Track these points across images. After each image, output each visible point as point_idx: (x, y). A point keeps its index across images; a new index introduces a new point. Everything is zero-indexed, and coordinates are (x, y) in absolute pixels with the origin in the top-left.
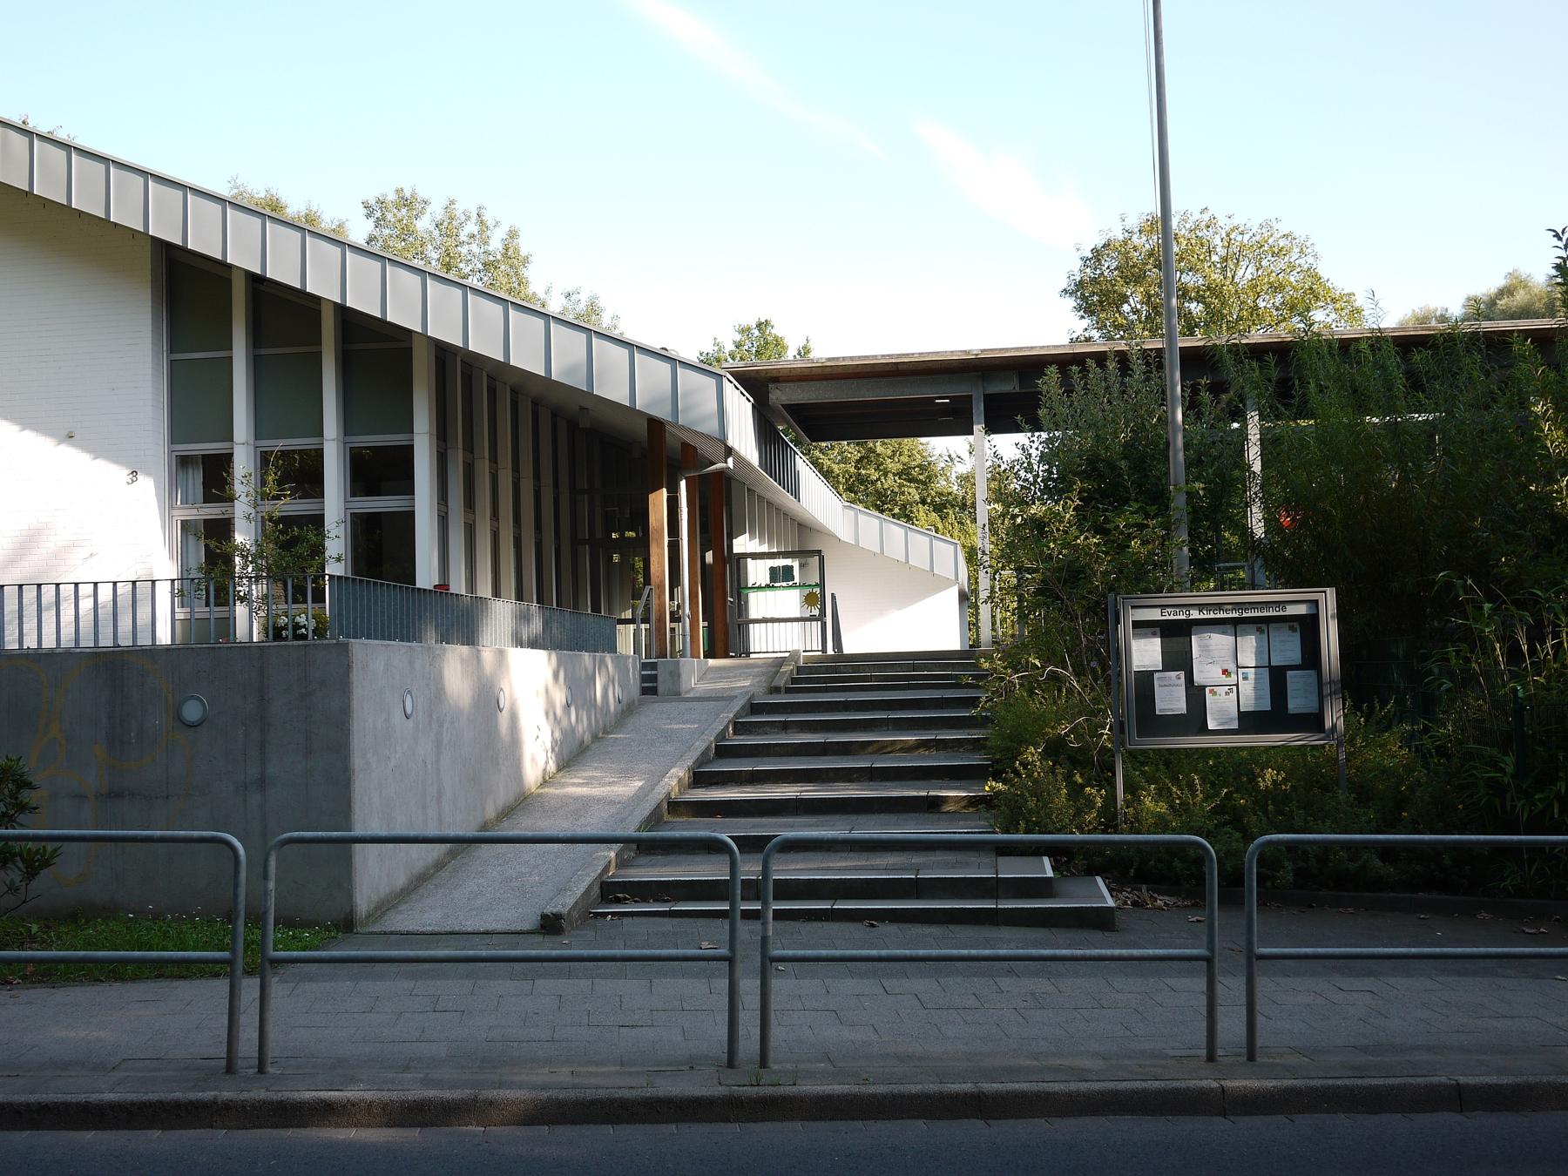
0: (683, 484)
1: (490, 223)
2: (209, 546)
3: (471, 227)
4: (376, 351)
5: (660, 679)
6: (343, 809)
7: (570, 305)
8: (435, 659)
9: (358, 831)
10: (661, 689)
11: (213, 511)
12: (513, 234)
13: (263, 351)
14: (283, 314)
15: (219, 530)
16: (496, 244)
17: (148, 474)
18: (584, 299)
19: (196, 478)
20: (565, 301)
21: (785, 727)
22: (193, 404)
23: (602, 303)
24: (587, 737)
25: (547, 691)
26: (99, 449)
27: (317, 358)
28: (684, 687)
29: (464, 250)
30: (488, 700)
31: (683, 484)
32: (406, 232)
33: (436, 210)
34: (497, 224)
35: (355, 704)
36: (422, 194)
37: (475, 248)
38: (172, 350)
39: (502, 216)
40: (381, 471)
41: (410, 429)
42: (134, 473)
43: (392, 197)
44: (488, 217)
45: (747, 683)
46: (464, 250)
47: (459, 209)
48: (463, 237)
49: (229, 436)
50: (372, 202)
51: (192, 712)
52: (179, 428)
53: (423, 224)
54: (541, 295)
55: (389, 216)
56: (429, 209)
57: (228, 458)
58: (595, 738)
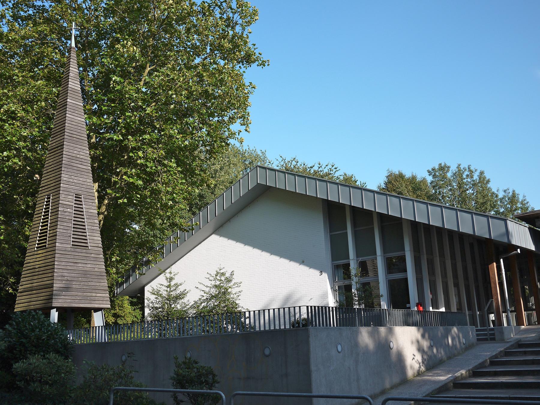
0: (502, 260)
1: (474, 170)
2: (344, 292)
3: (467, 173)
4: (391, 225)
5: (496, 334)
6: (309, 386)
7: (506, 195)
8: (357, 333)
9: (314, 394)
10: (497, 339)
11: (347, 282)
12: (482, 173)
13: (357, 229)
14: (361, 216)
15: (348, 288)
16: (476, 177)
17: (325, 272)
18: (511, 191)
19: (342, 271)
20: (504, 194)
21: (525, 353)
22: (338, 250)
23: (517, 192)
24: (445, 357)
25: (418, 342)
26: (311, 265)
27: (373, 229)
28: (506, 337)
29: (465, 181)
30: (384, 347)
31: (502, 260)
32: (444, 177)
33: (453, 168)
34: (476, 170)
35: (311, 349)
36: (448, 165)
37: (469, 180)
38: (331, 232)
39: (477, 166)
40: (395, 265)
41: (404, 250)
42: (321, 272)
43: (437, 167)
44: (472, 168)
45: (534, 335)
46: (465, 181)
47: (462, 167)
48: (464, 176)
49: (348, 258)
50: (430, 170)
51: (267, 352)
52: (334, 257)
53: (449, 175)
54: (496, 192)
55: (437, 174)
56: (451, 169)
57: (349, 265)
58: (449, 358)
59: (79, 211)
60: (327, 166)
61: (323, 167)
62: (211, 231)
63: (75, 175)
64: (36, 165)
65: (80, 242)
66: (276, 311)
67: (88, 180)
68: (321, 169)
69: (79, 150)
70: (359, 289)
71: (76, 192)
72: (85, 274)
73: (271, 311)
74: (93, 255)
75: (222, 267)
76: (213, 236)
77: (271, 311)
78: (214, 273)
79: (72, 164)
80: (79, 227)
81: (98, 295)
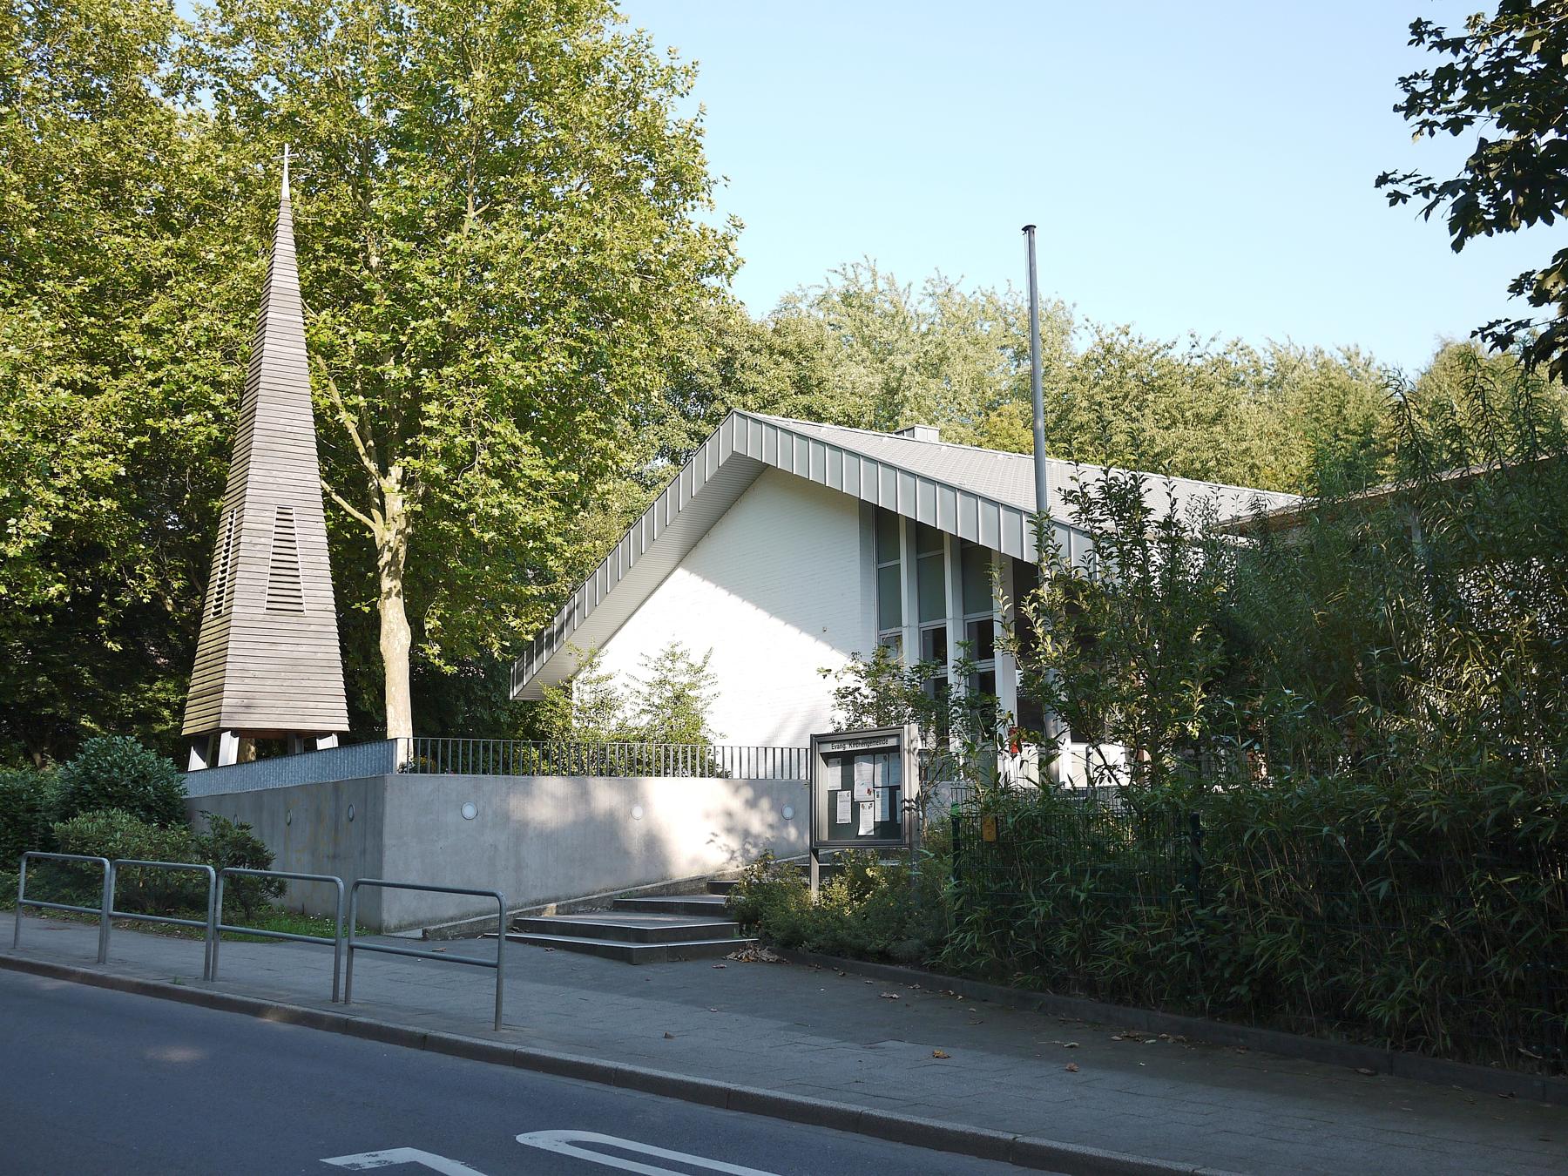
59: (285, 541)
60: (1213, 340)
61: (1202, 344)
62: (675, 558)
63: (280, 468)
64: (221, 450)
65: (285, 602)
66: (786, 752)
67: (310, 477)
68: (1197, 351)
69: (291, 416)
70: (39, 792)
71: (281, 502)
72: (295, 664)
73: (778, 752)
74: (313, 628)
75: (677, 640)
76: (680, 572)
77: (778, 752)
78: (655, 654)
79: (274, 447)
80: (285, 569)
81: (321, 705)
